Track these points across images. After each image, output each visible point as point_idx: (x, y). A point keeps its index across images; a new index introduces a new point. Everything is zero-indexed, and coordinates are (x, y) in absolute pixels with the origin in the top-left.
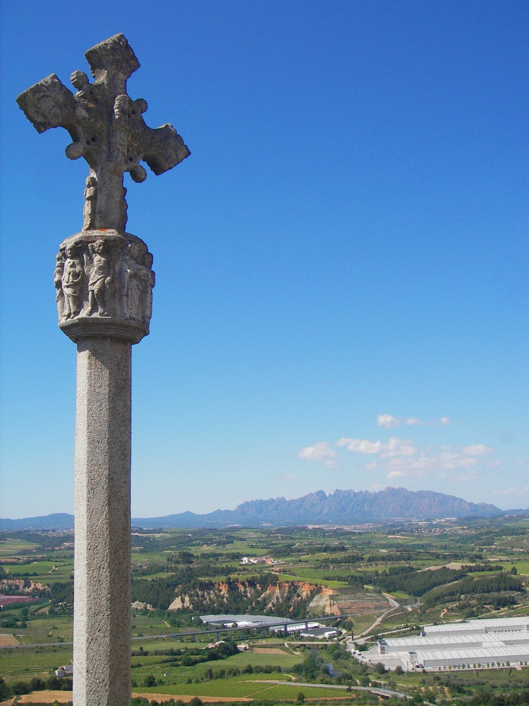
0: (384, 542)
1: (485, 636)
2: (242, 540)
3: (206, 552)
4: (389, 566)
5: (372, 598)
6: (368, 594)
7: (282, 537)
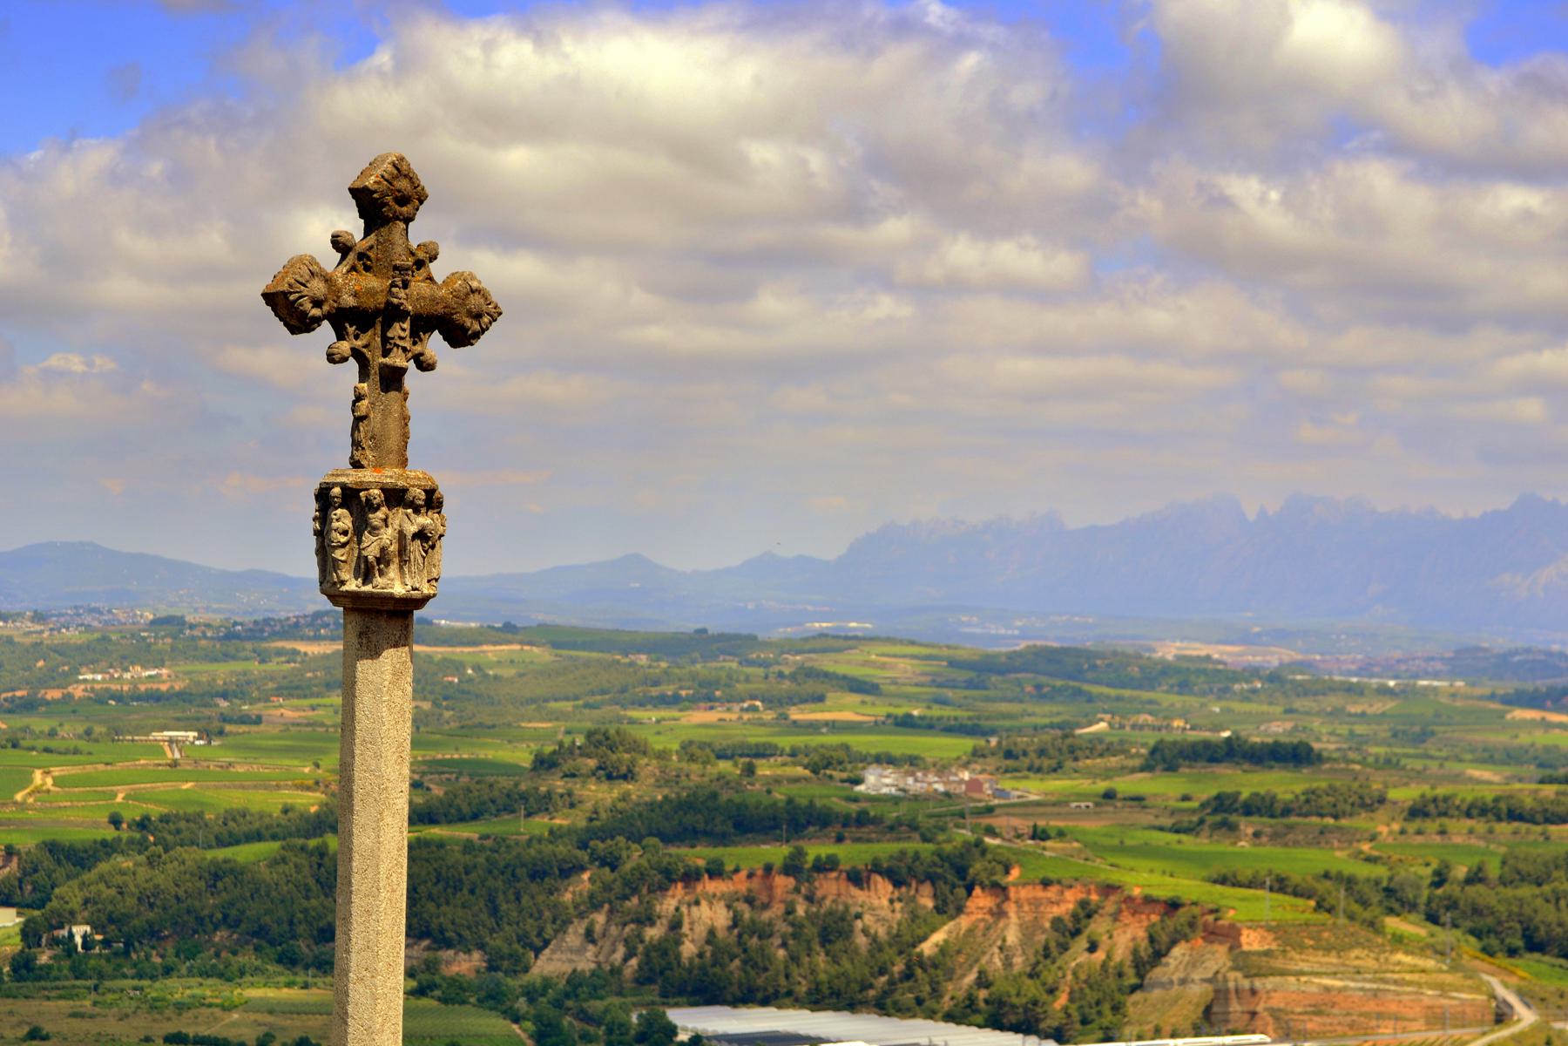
0: (1500, 739)
5: (1416, 977)
6: (1400, 957)
7: (1038, 687)
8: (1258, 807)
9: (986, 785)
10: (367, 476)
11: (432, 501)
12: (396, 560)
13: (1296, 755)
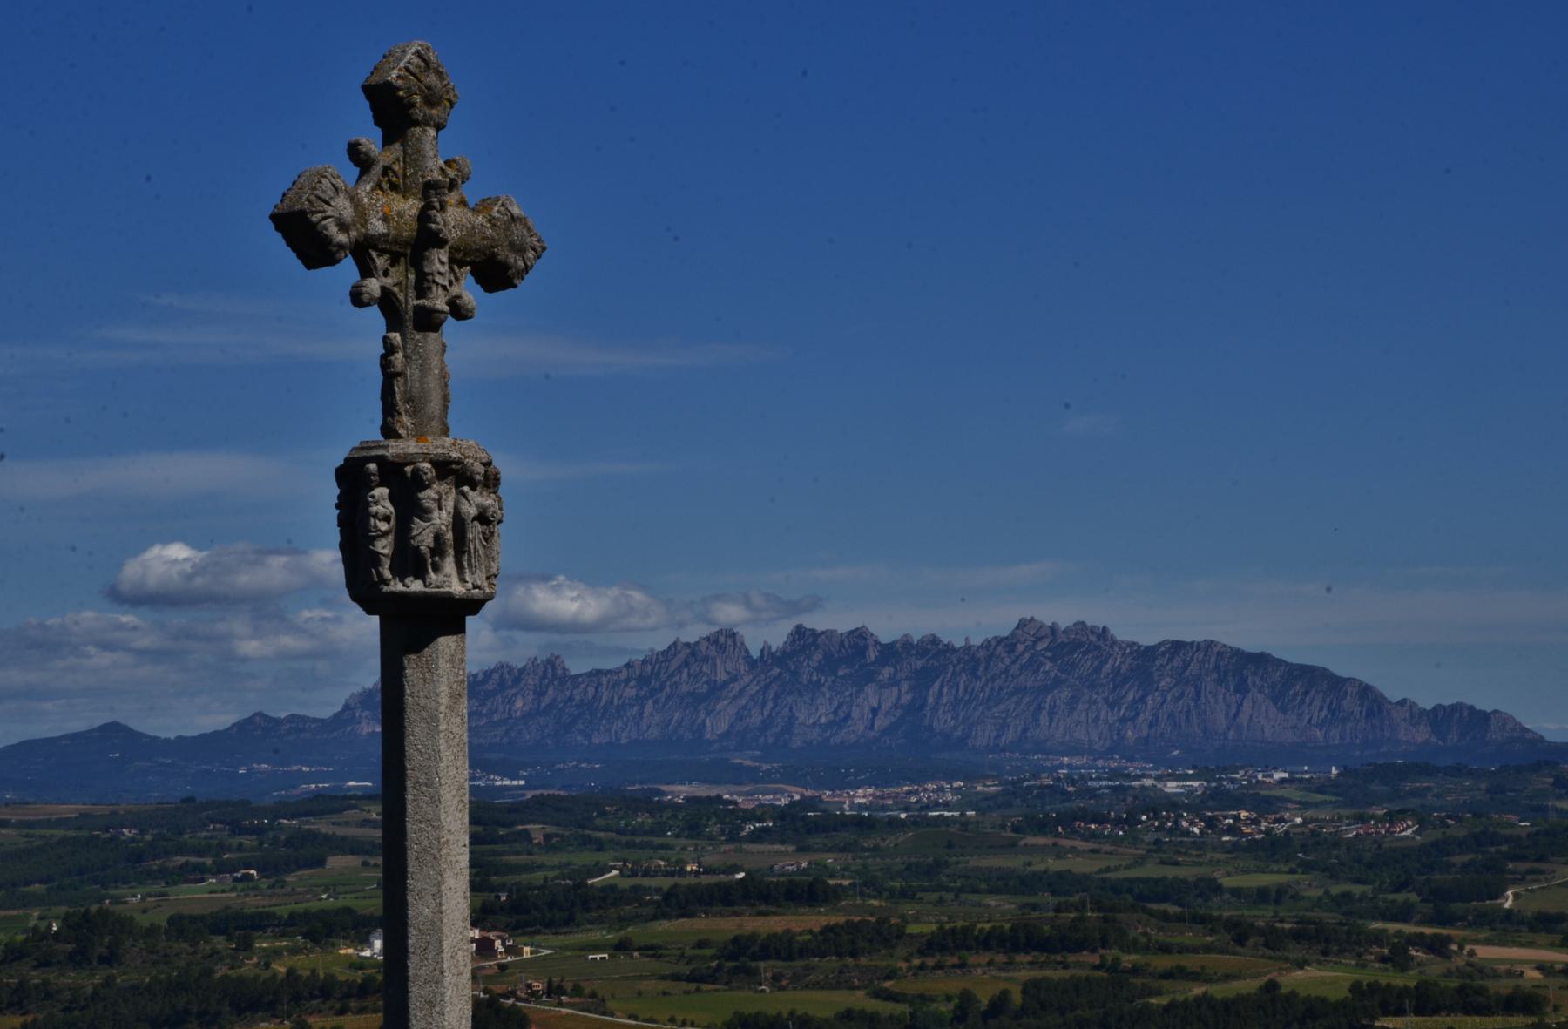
1: (1164, 982)
3: (197, 910)
4: (1024, 975)
8: (779, 948)
9: (498, 943)
10: (409, 446)
11: (491, 482)
12: (451, 551)
13: (808, 893)
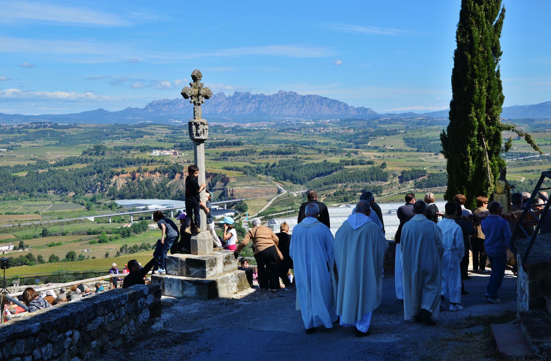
2: (152, 134)
6: (260, 182)
